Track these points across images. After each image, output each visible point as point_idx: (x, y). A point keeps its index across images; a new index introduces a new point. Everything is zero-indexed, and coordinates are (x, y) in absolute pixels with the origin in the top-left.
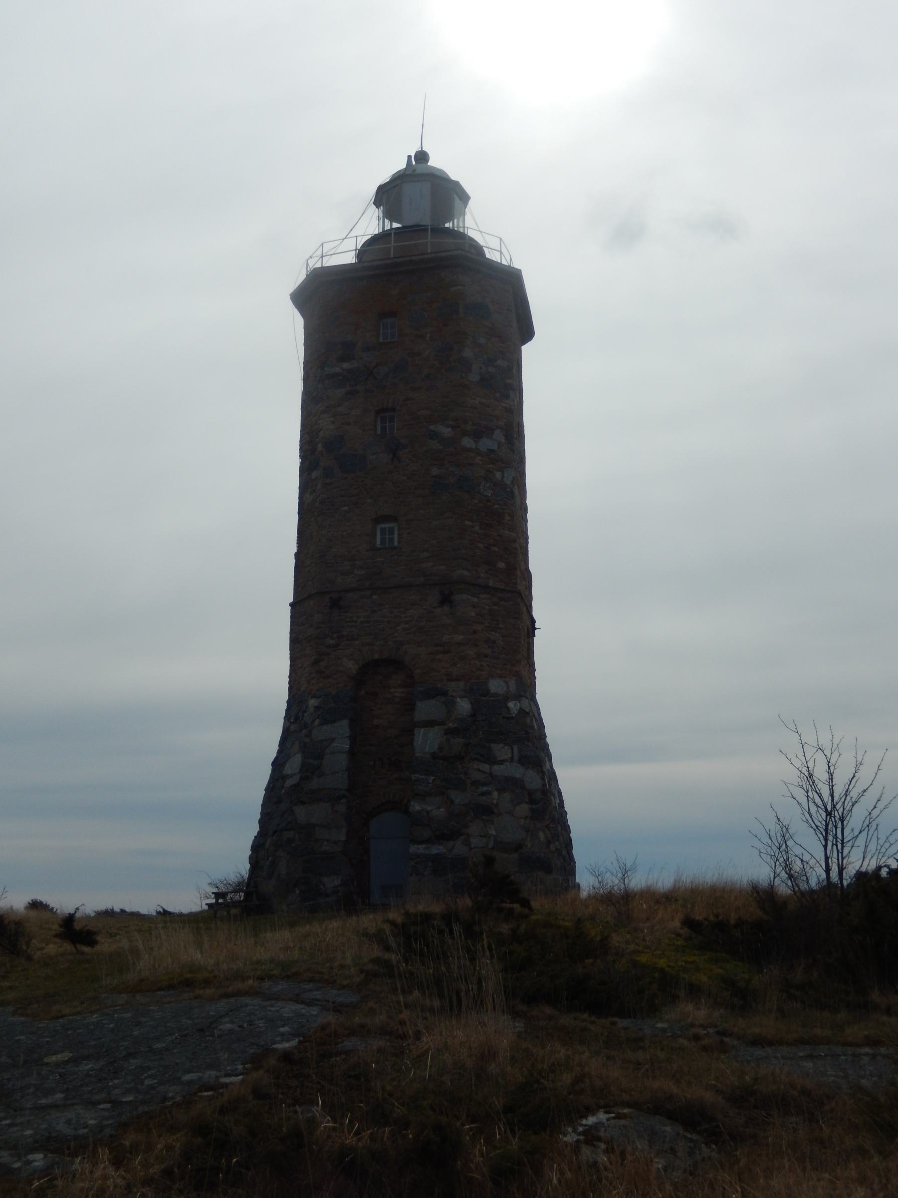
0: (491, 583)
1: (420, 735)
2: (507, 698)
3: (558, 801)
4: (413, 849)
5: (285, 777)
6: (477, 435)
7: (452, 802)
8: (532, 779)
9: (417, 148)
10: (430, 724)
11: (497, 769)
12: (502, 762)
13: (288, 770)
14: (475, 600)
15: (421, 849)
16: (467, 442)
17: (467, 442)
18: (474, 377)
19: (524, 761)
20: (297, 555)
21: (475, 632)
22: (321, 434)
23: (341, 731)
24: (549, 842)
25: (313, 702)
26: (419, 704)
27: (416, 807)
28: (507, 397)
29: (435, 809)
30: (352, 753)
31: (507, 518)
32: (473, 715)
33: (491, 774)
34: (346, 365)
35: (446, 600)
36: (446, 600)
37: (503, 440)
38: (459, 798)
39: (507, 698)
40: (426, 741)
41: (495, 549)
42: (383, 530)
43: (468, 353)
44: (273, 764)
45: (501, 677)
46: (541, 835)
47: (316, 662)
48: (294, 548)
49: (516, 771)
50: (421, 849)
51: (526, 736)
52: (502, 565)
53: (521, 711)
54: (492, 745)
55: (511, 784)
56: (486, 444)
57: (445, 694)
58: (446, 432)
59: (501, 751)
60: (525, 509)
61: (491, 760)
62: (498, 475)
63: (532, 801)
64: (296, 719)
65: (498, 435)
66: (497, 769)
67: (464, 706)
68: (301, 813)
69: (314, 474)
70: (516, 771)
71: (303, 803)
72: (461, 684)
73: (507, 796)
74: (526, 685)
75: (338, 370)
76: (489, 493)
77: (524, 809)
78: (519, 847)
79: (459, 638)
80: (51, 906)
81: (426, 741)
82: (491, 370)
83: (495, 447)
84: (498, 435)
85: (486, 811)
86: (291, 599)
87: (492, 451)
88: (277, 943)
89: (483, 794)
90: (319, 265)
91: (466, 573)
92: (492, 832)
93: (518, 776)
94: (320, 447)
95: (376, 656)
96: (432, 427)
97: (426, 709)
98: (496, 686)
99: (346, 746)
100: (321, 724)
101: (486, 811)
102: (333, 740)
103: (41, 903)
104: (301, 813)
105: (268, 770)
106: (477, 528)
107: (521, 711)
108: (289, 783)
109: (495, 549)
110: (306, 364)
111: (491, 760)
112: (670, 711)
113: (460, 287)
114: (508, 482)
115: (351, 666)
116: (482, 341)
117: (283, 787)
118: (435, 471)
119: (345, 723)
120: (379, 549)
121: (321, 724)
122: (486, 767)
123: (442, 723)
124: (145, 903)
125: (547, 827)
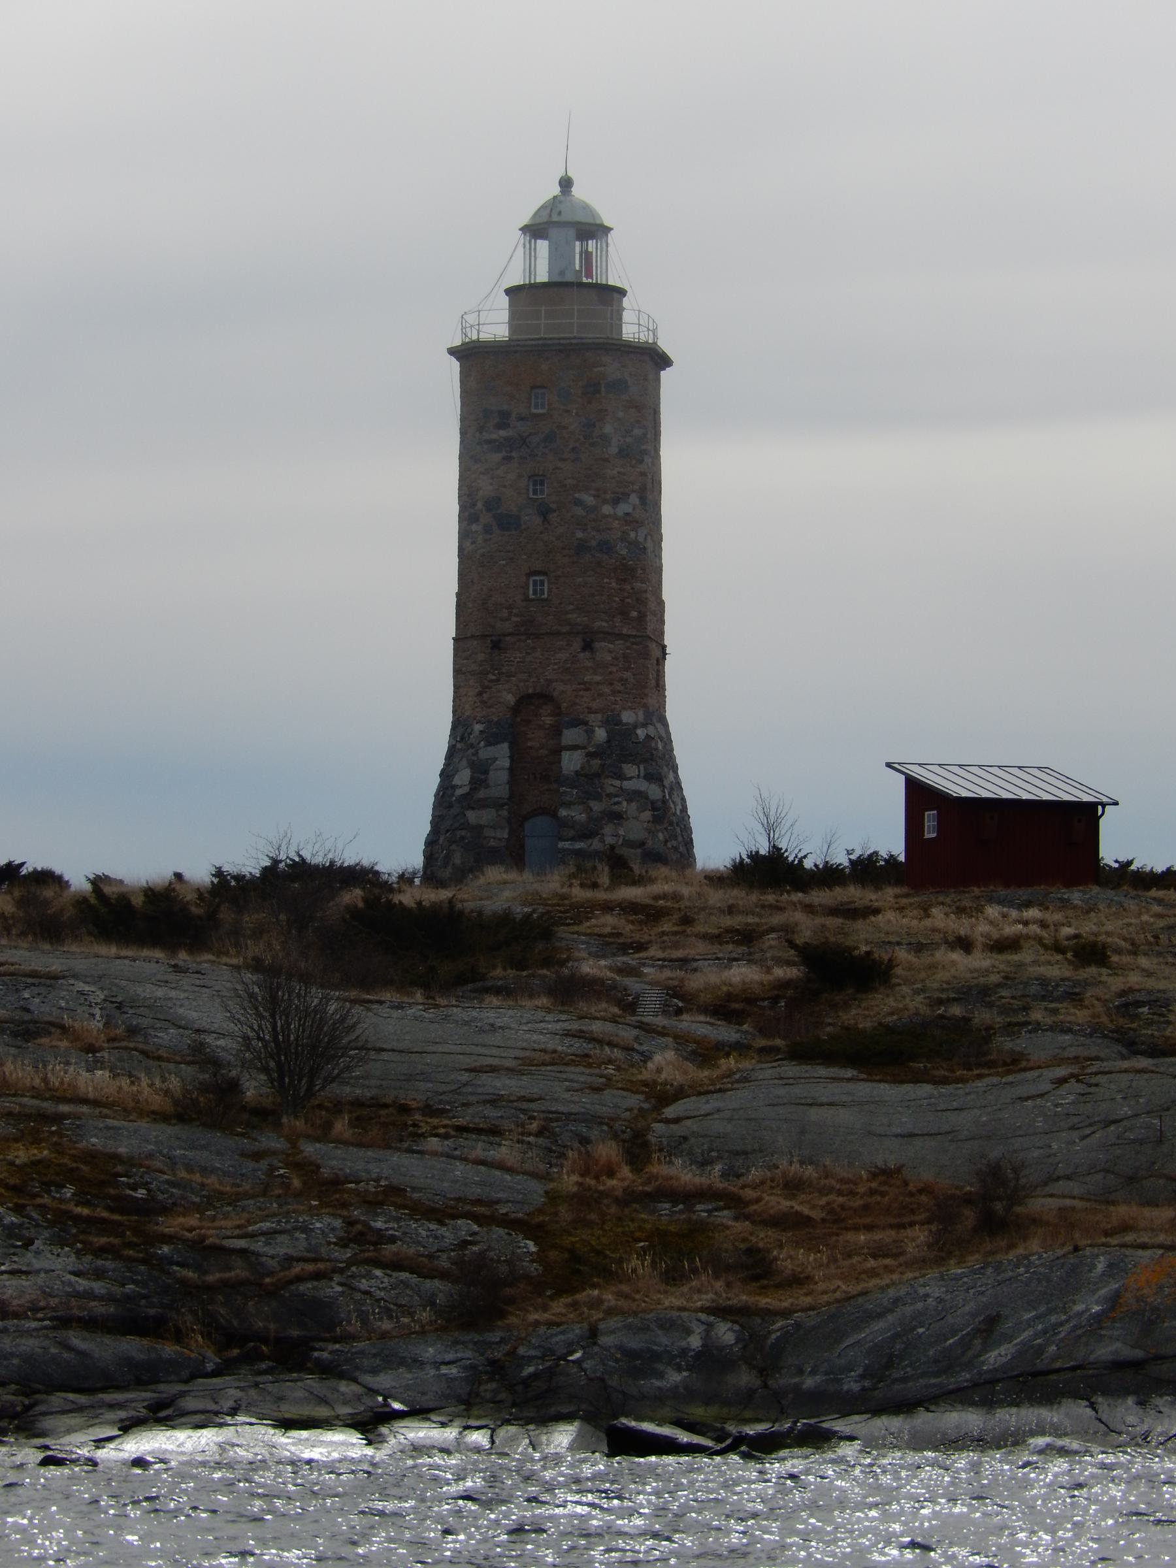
0: (625, 631)
1: (566, 755)
2: (635, 727)
3: (679, 807)
4: (561, 845)
5: (455, 787)
6: (616, 502)
7: (591, 810)
8: (654, 792)
9: (562, 173)
10: (575, 748)
11: (627, 784)
12: (630, 779)
13: (457, 781)
14: (611, 646)
15: (566, 845)
16: (607, 509)
17: (607, 509)
18: (614, 450)
19: (649, 777)
20: (458, 595)
21: (611, 673)
22: (481, 493)
23: (501, 754)
24: (666, 841)
25: (478, 727)
26: (566, 732)
27: (563, 813)
28: (641, 461)
29: (577, 814)
30: (511, 770)
31: (640, 571)
32: (608, 742)
33: (621, 788)
34: (503, 433)
35: (588, 646)
36: (588, 646)
37: (637, 502)
38: (596, 806)
39: (635, 727)
40: (571, 762)
41: (629, 600)
42: (535, 582)
43: (608, 429)
44: (441, 775)
45: (631, 709)
46: (661, 836)
47: (480, 694)
48: (455, 588)
49: (642, 785)
50: (566, 845)
51: (657, 759)
52: (634, 614)
53: (648, 736)
54: (624, 765)
55: (637, 795)
56: (623, 508)
57: (586, 723)
58: (589, 499)
59: (630, 770)
60: (659, 570)
61: (621, 777)
62: (632, 534)
63: (654, 809)
64: (462, 739)
65: (634, 499)
66: (627, 784)
67: (601, 734)
68: (472, 817)
69: (474, 527)
70: (642, 785)
71: (473, 809)
72: (599, 716)
73: (634, 805)
74: (657, 715)
75: (494, 436)
76: (624, 552)
77: (647, 815)
78: (642, 844)
79: (598, 678)
80: (66, 878)
81: (571, 762)
82: (628, 440)
83: (630, 510)
84: (634, 499)
85: (617, 817)
86: (453, 633)
87: (627, 514)
88: (737, 895)
89: (615, 804)
90: (475, 337)
91: (604, 624)
92: (621, 832)
93: (643, 789)
94: (480, 505)
95: (530, 691)
96: (577, 495)
97: (571, 736)
98: (627, 717)
99: (507, 764)
100: (486, 746)
101: (617, 817)
102: (496, 759)
103: (107, 877)
104: (472, 817)
105: (437, 780)
106: (614, 584)
107: (648, 736)
108: (459, 792)
109: (629, 600)
110: (463, 419)
111: (621, 777)
112: (787, 719)
113: (602, 369)
114: (641, 539)
115: (510, 699)
116: (621, 414)
117: (453, 795)
118: (579, 535)
119: (505, 745)
120: (533, 600)
121: (486, 746)
122: (617, 783)
123: (584, 748)
124: (113, 876)
125: (666, 829)
